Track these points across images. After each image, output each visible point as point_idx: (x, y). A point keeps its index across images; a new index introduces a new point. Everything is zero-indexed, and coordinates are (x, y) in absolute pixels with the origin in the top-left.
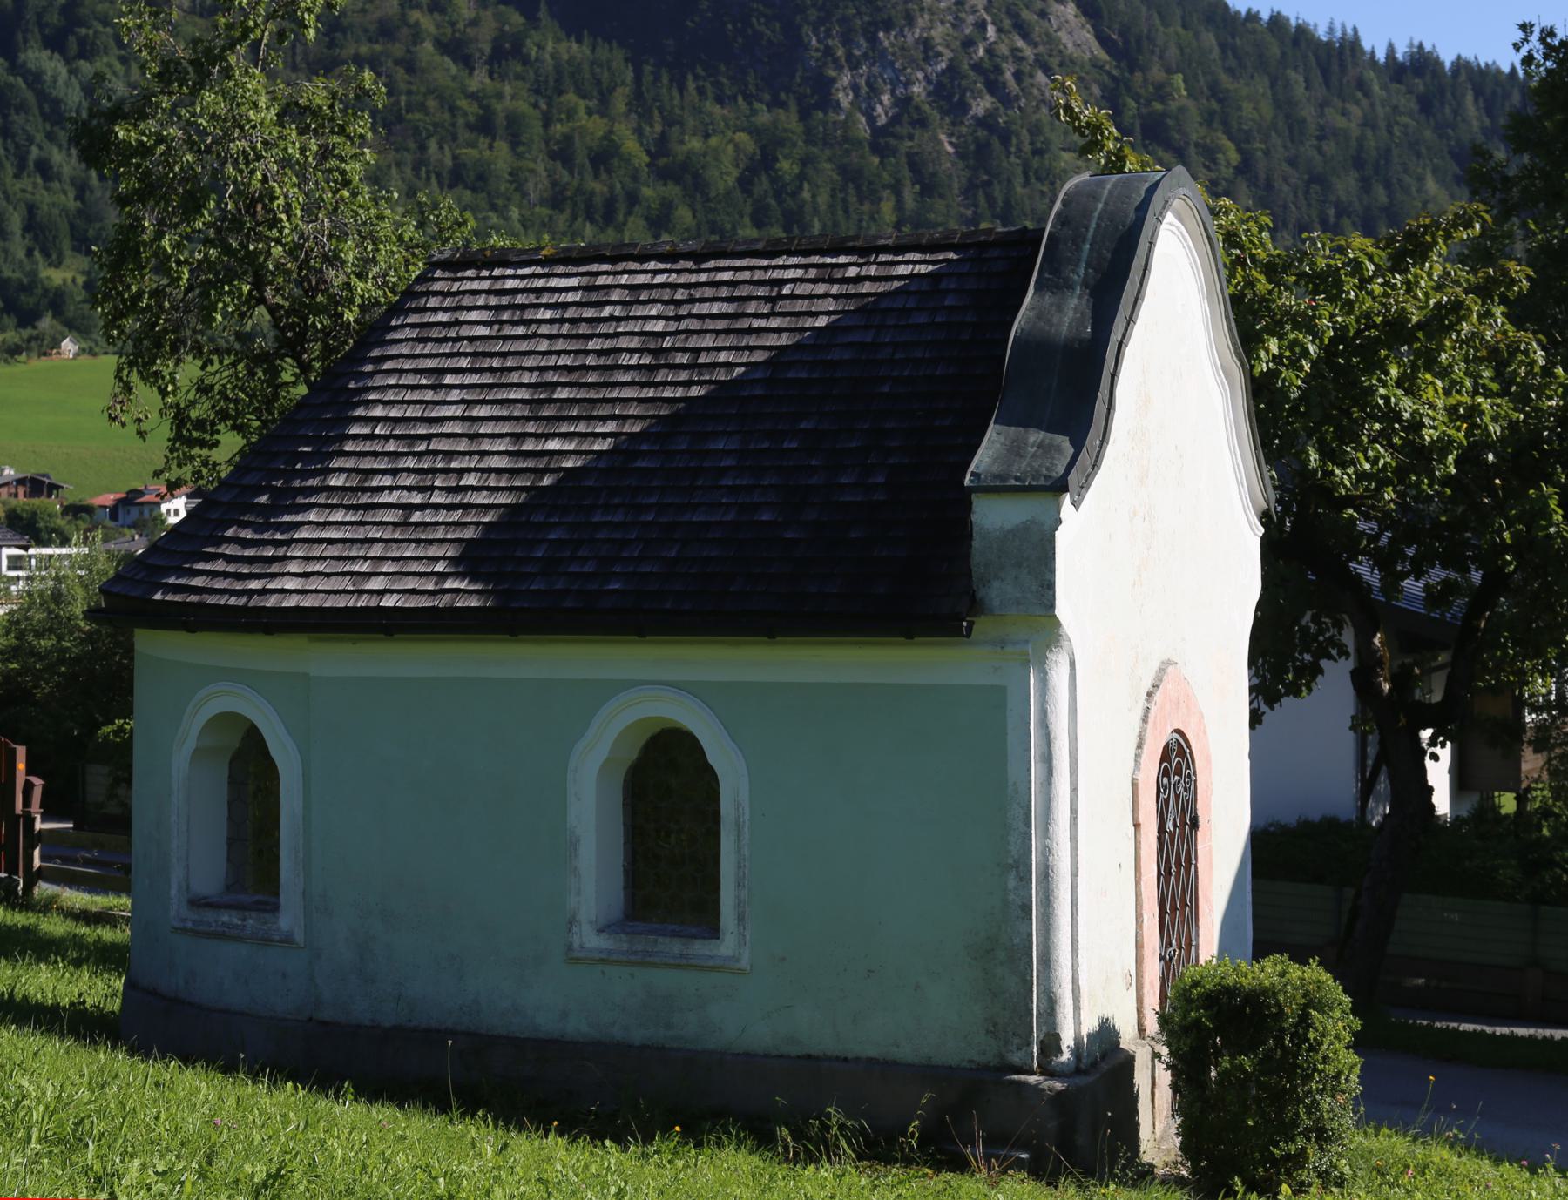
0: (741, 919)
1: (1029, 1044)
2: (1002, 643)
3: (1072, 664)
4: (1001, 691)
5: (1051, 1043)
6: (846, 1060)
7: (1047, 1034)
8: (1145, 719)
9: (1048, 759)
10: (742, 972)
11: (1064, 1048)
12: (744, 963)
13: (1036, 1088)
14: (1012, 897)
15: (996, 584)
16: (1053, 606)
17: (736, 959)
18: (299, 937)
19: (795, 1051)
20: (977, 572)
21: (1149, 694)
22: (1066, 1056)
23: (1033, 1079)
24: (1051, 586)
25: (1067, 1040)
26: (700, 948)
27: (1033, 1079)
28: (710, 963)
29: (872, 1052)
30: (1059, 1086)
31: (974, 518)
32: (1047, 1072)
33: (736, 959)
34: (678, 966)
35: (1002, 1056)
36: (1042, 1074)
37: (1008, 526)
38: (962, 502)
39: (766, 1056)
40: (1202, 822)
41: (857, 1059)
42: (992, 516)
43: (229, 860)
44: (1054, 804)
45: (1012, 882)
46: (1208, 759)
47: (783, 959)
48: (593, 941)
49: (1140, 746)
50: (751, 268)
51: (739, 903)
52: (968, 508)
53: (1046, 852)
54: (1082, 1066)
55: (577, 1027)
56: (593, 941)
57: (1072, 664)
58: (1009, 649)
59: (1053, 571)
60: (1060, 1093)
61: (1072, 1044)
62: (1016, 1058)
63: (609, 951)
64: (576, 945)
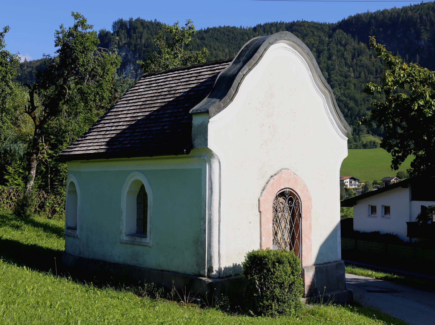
0: (150, 233)
1: (205, 269)
2: (200, 156)
3: (220, 163)
4: (200, 170)
5: (210, 269)
6: (169, 271)
7: (210, 266)
8: (267, 183)
9: (211, 189)
10: (150, 247)
11: (214, 270)
12: (150, 245)
13: (204, 281)
14: (202, 227)
15: (196, 140)
16: (207, 145)
17: (149, 243)
18: (79, 236)
19: (159, 268)
20: (193, 136)
21: (272, 176)
22: (214, 273)
23: (204, 279)
24: (206, 139)
25: (216, 268)
26: (143, 240)
27: (204, 279)
28: (144, 244)
29: (174, 269)
30: (210, 281)
31: (193, 122)
32: (209, 277)
33: (149, 243)
34: (139, 245)
35: (199, 272)
36: (208, 277)
37: (199, 124)
38: (190, 117)
39: (154, 270)
40: (303, 215)
41: (171, 271)
42: (196, 121)
43: (137, 225)
44: (213, 201)
45: (202, 223)
46: (310, 199)
47: (158, 244)
48: (125, 238)
49: (263, 190)
50: (194, 70)
51: (150, 229)
52: (192, 119)
53: (210, 215)
54: (221, 276)
55: (121, 260)
56: (125, 238)
57: (220, 163)
58: (201, 158)
59: (207, 135)
60: (210, 283)
61: (217, 270)
62: (202, 273)
63: (127, 241)
64: (121, 239)
